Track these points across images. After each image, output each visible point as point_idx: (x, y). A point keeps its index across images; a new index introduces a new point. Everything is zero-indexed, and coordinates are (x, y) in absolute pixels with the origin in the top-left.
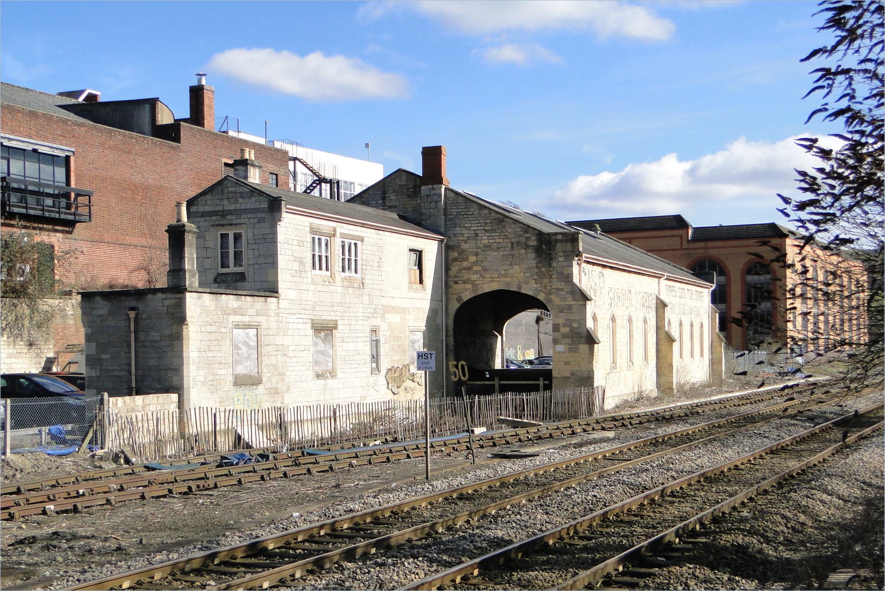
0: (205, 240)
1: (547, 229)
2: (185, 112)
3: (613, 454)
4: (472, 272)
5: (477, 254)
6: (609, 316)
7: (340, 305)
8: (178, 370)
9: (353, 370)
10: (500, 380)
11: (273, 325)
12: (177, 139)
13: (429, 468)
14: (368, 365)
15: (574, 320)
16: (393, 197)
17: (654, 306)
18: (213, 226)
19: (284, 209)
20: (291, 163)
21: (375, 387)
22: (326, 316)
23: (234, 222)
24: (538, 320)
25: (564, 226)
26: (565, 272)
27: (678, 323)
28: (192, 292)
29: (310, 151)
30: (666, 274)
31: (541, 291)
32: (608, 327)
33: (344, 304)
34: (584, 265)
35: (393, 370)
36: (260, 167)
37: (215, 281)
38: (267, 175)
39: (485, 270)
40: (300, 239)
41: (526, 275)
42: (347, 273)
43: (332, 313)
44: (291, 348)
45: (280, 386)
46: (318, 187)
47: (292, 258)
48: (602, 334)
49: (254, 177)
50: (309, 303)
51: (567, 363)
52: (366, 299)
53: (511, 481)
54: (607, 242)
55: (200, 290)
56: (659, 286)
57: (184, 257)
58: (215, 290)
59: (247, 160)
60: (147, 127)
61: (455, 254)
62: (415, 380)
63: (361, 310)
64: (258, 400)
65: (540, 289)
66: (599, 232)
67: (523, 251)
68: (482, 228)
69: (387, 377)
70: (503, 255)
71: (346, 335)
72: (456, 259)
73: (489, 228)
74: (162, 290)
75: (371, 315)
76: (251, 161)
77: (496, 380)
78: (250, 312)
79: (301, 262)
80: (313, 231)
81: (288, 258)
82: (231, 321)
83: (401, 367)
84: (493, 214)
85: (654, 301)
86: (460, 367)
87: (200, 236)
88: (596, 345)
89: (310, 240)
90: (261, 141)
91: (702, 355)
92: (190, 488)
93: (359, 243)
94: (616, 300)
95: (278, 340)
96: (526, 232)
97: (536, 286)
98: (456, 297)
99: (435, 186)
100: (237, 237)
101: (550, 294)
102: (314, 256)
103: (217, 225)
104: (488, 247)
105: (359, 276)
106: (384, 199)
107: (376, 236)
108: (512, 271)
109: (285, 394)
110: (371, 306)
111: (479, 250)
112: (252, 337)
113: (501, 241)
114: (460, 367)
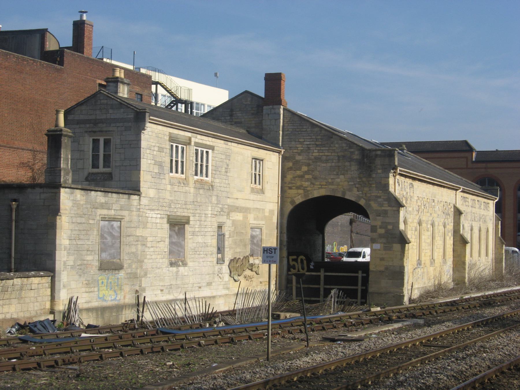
0: (79, 144)
1: (367, 147)
2: (67, 41)
3: (428, 340)
4: (304, 179)
5: (308, 165)
6: (416, 221)
7: (192, 203)
8: (51, 255)
9: (201, 260)
10: (325, 271)
11: (135, 218)
12: (61, 63)
13: (270, 352)
14: (215, 255)
15: (389, 223)
16: (239, 115)
17: (452, 214)
18: (86, 132)
19: (147, 120)
20: (153, 87)
21: (220, 275)
22: (181, 213)
23: (105, 129)
24: (351, 222)
25: (378, 145)
26: (383, 182)
27: (486, 230)
28: (66, 188)
29: (174, 78)
30: (462, 187)
31: (362, 197)
32: (416, 230)
33: (195, 203)
34: (398, 177)
35: (235, 261)
36: (128, 84)
37: (87, 179)
38: (134, 95)
39: (315, 178)
40: (161, 146)
41: (350, 183)
42: (198, 177)
43: (185, 210)
44: (149, 239)
45: (139, 271)
46: (175, 106)
47: (153, 162)
48: (411, 235)
49: (124, 92)
50: (167, 201)
51: (382, 259)
52: (214, 199)
53: (344, 365)
54: (411, 157)
55: (73, 186)
56: (456, 197)
57: (60, 158)
58: (85, 187)
59: (117, 78)
60: (37, 52)
61: (290, 164)
62: (254, 269)
63: (210, 208)
64: (119, 283)
65: (361, 195)
66: (405, 151)
67: (347, 164)
68: (313, 143)
69: (230, 267)
70: (331, 167)
71: (197, 230)
72: (291, 169)
73: (320, 143)
74: (40, 186)
75: (218, 214)
76: (122, 79)
77: (322, 271)
78: (115, 207)
79: (160, 165)
80: (172, 139)
81: (149, 162)
82: (98, 214)
83: (242, 258)
84: (323, 132)
85: (452, 209)
86: (299, 260)
87: (75, 140)
88: (407, 245)
89: (169, 147)
90: (131, 67)
91: (487, 255)
92: (56, 362)
93: (210, 151)
94: (423, 207)
95: (139, 232)
96: (350, 147)
97: (358, 193)
98: (289, 200)
99: (275, 106)
100: (107, 143)
101: (370, 200)
102: (172, 160)
103: (90, 132)
104: (318, 159)
105: (209, 179)
106: (231, 116)
107: (224, 146)
108: (338, 180)
109: (143, 279)
110: (219, 205)
111: (311, 162)
112: (117, 229)
113: (329, 154)
114: (299, 260)
